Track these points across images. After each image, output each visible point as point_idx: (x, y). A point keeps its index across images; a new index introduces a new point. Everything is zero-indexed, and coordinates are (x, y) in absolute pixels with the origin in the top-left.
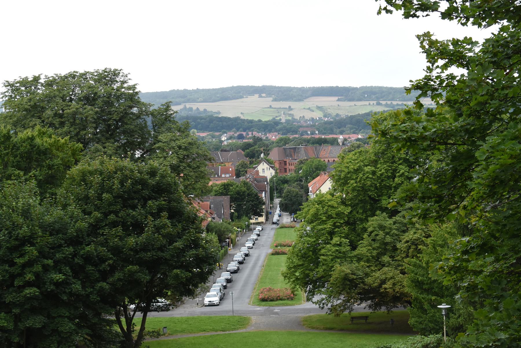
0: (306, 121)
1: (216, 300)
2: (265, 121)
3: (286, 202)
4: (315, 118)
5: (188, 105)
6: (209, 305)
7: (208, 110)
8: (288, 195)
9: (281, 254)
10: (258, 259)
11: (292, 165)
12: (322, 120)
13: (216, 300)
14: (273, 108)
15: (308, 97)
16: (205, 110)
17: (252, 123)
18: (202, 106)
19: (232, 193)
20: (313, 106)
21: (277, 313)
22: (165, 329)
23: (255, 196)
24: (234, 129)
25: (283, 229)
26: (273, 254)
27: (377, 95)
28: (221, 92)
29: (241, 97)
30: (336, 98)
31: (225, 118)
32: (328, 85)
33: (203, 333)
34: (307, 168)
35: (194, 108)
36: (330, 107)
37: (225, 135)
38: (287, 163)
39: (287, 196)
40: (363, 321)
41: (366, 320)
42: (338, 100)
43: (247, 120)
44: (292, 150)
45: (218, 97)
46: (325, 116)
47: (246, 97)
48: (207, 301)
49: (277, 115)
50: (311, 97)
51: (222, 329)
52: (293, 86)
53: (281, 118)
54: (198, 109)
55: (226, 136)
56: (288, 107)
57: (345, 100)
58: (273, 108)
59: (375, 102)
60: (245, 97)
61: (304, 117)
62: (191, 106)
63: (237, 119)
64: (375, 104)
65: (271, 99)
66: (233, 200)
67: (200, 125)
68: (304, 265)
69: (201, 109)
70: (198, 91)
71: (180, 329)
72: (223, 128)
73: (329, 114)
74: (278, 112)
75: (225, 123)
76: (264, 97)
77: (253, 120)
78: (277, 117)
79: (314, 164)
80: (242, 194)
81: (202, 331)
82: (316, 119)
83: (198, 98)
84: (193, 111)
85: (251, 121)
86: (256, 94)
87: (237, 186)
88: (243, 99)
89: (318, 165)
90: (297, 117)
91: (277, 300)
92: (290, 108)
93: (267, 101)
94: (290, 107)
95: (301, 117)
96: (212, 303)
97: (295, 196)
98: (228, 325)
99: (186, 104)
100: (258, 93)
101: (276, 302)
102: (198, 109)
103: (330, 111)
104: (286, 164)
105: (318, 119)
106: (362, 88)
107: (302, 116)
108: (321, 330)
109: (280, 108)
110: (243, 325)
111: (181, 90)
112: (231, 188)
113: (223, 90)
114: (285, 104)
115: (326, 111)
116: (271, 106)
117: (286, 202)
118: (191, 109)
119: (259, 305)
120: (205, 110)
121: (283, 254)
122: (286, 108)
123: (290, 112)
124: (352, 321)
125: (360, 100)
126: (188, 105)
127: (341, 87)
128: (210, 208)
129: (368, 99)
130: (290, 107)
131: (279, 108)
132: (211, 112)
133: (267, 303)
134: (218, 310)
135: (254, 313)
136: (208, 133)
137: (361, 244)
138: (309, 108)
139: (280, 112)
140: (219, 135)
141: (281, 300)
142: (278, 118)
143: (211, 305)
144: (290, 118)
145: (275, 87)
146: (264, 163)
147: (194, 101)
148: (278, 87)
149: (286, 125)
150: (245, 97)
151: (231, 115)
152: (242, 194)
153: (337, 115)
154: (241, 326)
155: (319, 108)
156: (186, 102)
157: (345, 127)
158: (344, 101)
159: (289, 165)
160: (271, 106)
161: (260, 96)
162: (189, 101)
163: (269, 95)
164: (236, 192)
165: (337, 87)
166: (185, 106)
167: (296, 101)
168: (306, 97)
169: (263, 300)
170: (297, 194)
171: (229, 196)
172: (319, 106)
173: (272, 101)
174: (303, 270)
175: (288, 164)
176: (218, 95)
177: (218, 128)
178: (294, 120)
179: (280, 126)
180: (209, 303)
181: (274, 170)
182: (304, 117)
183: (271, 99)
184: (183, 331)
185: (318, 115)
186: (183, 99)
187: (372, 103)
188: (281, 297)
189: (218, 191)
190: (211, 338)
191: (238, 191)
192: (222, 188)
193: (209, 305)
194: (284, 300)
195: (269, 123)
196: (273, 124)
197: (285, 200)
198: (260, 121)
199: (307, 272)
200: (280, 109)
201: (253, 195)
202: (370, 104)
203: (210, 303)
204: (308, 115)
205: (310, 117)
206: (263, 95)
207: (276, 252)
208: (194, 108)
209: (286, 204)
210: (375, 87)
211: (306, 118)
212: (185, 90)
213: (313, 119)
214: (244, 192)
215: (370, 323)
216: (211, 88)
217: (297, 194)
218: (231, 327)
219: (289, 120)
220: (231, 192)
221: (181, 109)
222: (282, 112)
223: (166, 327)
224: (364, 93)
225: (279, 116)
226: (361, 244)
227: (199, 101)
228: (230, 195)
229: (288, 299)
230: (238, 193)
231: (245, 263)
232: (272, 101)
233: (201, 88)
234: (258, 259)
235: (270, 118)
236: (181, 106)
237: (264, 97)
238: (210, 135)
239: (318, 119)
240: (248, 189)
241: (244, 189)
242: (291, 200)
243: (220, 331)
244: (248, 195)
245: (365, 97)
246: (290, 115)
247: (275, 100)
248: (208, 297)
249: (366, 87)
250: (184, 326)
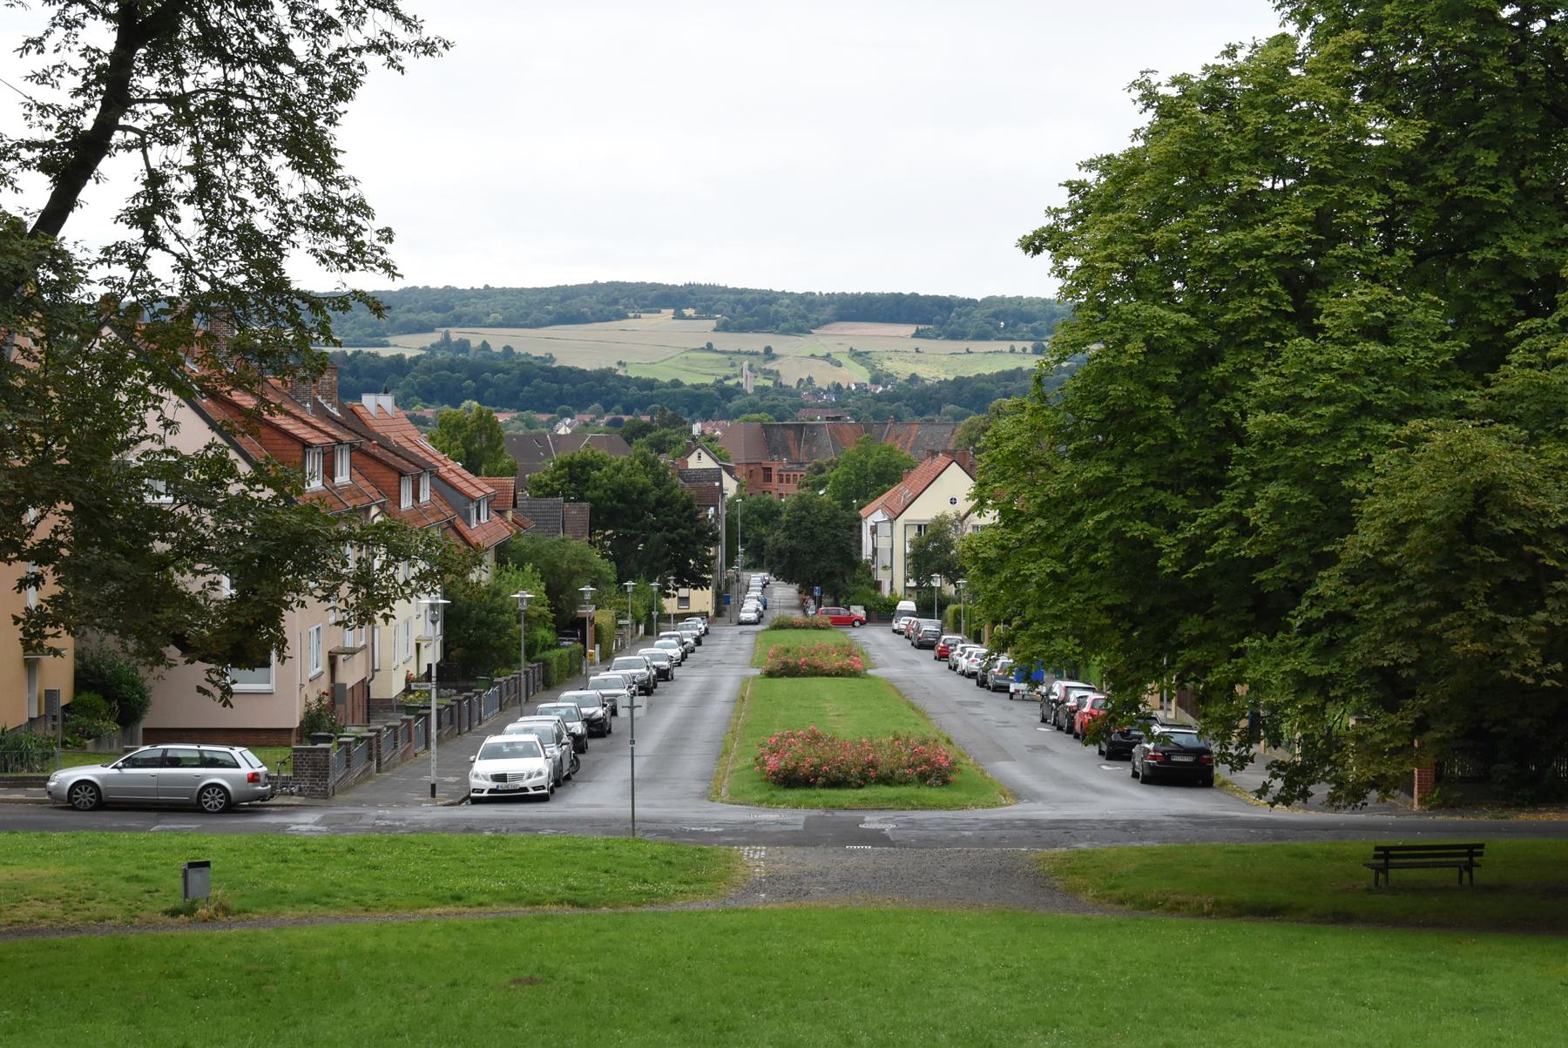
0: (817, 393)
1: (533, 769)
2: (693, 386)
3: (794, 542)
4: (845, 387)
5: (456, 334)
6: (496, 798)
7: (516, 350)
8: (804, 517)
9: (805, 675)
10: (704, 696)
11: (788, 481)
12: (867, 391)
13: (533, 769)
14: (716, 351)
15: (826, 322)
16: (508, 350)
17: (652, 389)
18: (498, 339)
19: (599, 493)
20: (840, 348)
21: (877, 838)
22: (195, 876)
23: (685, 509)
24: (597, 405)
25: (783, 632)
26: (770, 674)
27: (1036, 324)
28: (557, 298)
29: (621, 316)
30: (912, 329)
31: (570, 370)
32: (887, 291)
33: (451, 908)
34: (847, 473)
35: (475, 342)
36: (891, 355)
37: (568, 421)
38: (774, 472)
39: (799, 523)
40: (1449, 875)
41: (1469, 867)
42: (917, 335)
43: (637, 378)
44: (791, 433)
45: (549, 313)
46: (876, 380)
47: (635, 317)
48: (483, 771)
49: (730, 372)
50: (832, 321)
51: (569, 895)
52: (779, 290)
53: (742, 380)
54: (485, 345)
55: (569, 426)
56: (762, 351)
57: (939, 335)
58: (716, 351)
59: (1029, 345)
60: (631, 315)
61: (810, 380)
62: (465, 337)
63: (604, 376)
64: (1029, 350)
65: (713, 324)
66: (600, 518)
67: (491, 390)
68: (1119, 482)
69: (497, 347)
70: (487, 293)
71: (306, 888)
72: (561, 399)
73: (889, 375)
74: (733, 365)
75: (566, 386)
76: (690, 318)
77: (655, 380)
78: (727, 378)
79: (871, 461)
80: (635, 497)
81: (442, 901)
82: (849, 388)
83: (488, 315)
84: (471, 353)
85: (649, 384)
86: (666, 307)
87: (618, 470)
88: (625, 322)
89: (886, 466)
90: (790, 380)
91: (864, 781)
92: (769, 354)
93: (702, 330)
94: (768, 350)
95: (801, 380)
96: (510, 785)
97: (826, 524)
98: (605, 878)
99: (450, 329)
100: (672, 307)
101: (862, 793)
102: (485, 345)
103: (890, 366)
104: (768, 478)
105: (854, 388)
106: (990, 301)
107: (805, 377)
108: (1199, 913)
109: (739, 352)
110: (699, 881)
111: (437, 291)
112: (596, 473)
113: (566, 294)
114: (755, 342)
115: (879, 367)
116: (710, 346)
117: (794, 542)
118: (464, 346)
119: (769, 803)
120: (508, 350)
121: (816, 675)
122: (757, 354)
123: (768, 366)
124: (1383, 869)
125: (983, 336)
126: (456, 334)
127: (927, 298)
128: (515, 505)
129: (1008, 335)
130: (768, 350)
131: (734, 353)
132: (527, 355)
133: (812, 792)
134: (551, 815)
135: (753, 835)
136: (516, 415)
137: (1522, 337)
138: (829, 355)
139: (737, 363)
140: (549, 421)
141: (886, 780)
142: (731, 383)
143: (507, 794)
144: (770, 383)
145: (725, 290)
146: (703, 454)
147: (476, 322)
148: (735, 291)
149: (756, 398)
150: (631, 315)
151: (588, 362)
152: (635, 497)
153: (914, 378)
154: (684, 887)
155: (859, 356)
156: (449, 325)
157: (939, 412)
158: (937, 337)
159: (781, 481)
160: (710, 346)
161: (679, 316)
162: (458, 321)
163: (706, 311)
164: (613, 491)
165: (915, 296)
166: (447, 335)
167: (786, 332)
168: (819, 324)
169: (790, 780)
170: (835, 516)
171: (586, 505)
172: (860, 350)
173: (715, 330)
174: (1110, 518)
175: (775, 478)
176: (550, 308)
177: (547, 401)
178: (781, 389)
179: (737, 402)
180: (494, 785)
181: (736, 479)
182: (810, 380)
183: (713, 324)
184: (321, 898)
185: (854, 375)
186: (440, 316)
187: (1019, 346)
188: (883, 770)
189: (546, 485)
190: (495, 932)
191: (622, 486)
192: (562, 477)
193: (496, 798)
194: (906, 783)
195: (703, 391)
196: (716, 394)
197: (791, 538)
198: (676, 383)
199: (1138, 529)
200: (737, 356)
201: (678, 506)
202: (1012, 351)
203: (502, 785)
204: (824, 377)
205: (830, 382)
206: (689, 312)
207: (785, 664)
208: (475, 342)
209: (793, 551)
210: (1031, 301)
211: (818, 384)
212: (449, 290)
213: (839, 386)
214: (644, 491)
215: (1489, 889)
216: (530, 286)
217: (835, 516)
218: (625, 886)
219: (766, 388)
220: (596, 488)
221: (433, 346)
222: (746, 364)
223: (207, 864)
224: (997, 316)
225: (735, 376)
226: (1522, 337)
227: (489, 321)
228: (591, 500)
229: (923, 778)
230: (621, 494)
231: (658, 694)
232: (715, 330)
233: (497, 284)
234: (704, 696)
235: (710, 381)
236: (433, 335)
237: (690, 318)
238: (522, 421)
239: (854, 388)
240: (658, 485)
241: (643, 480)
242: (812, 537)
243: (561, 902)
244: (660, 503)
245: (997, 328)
246: (768, 374)
247: (724, 327)
248: (495, 753)
249: (1002, 300)
250: (333, 873)
